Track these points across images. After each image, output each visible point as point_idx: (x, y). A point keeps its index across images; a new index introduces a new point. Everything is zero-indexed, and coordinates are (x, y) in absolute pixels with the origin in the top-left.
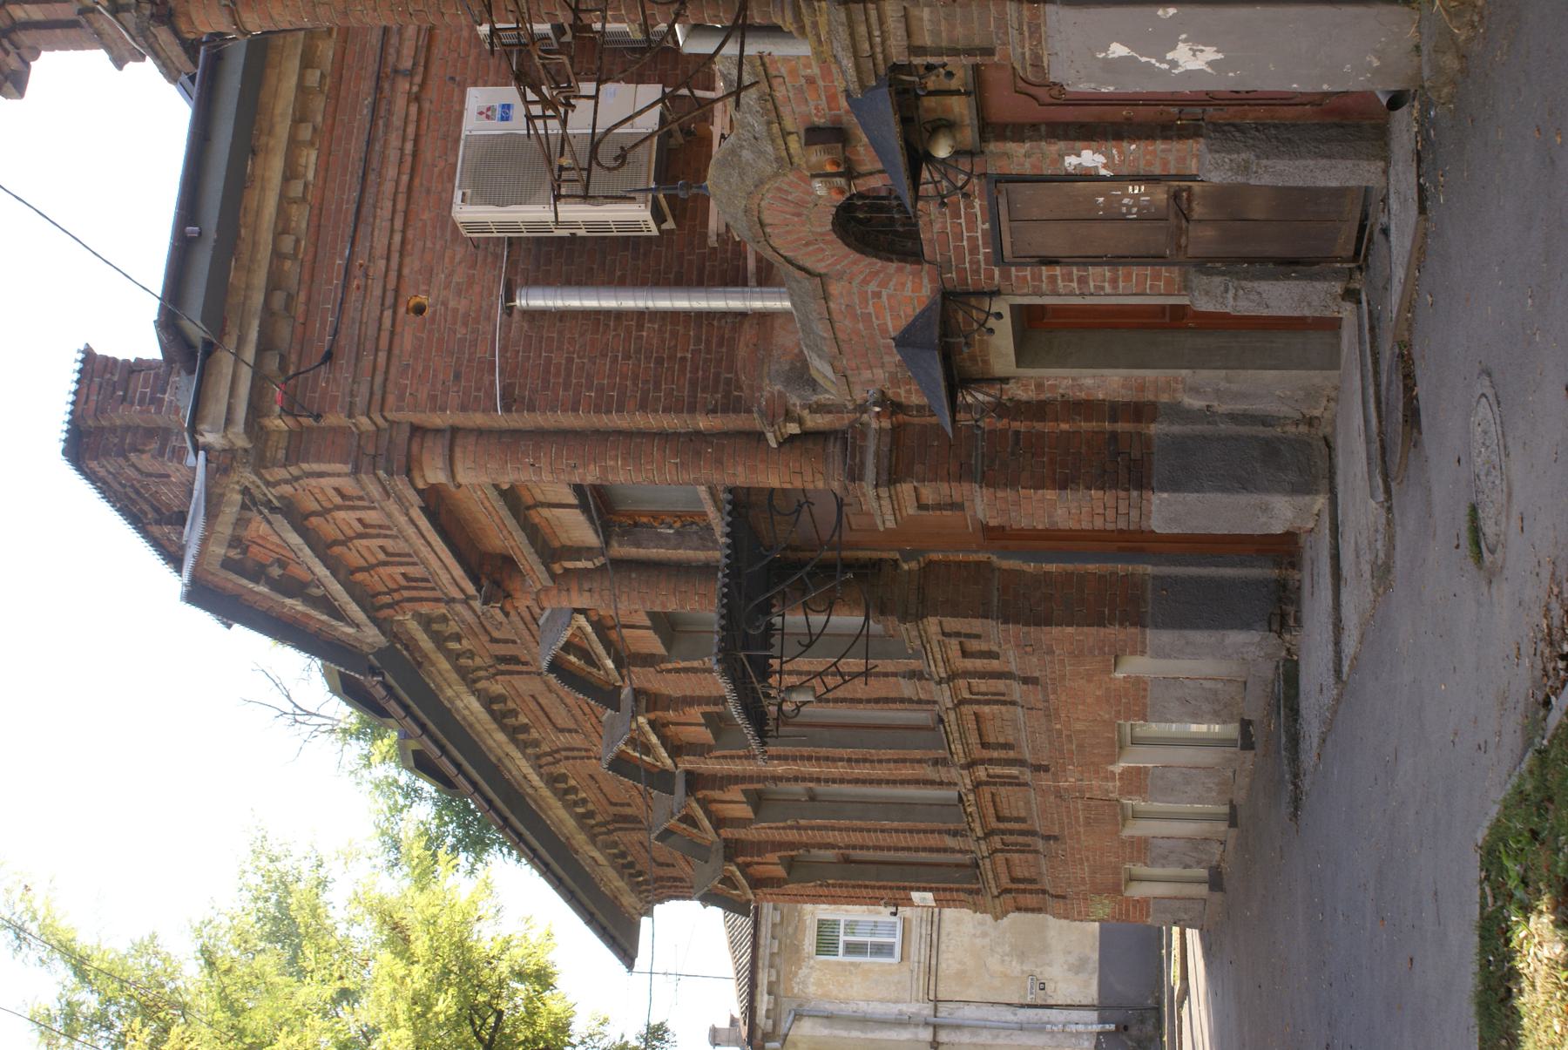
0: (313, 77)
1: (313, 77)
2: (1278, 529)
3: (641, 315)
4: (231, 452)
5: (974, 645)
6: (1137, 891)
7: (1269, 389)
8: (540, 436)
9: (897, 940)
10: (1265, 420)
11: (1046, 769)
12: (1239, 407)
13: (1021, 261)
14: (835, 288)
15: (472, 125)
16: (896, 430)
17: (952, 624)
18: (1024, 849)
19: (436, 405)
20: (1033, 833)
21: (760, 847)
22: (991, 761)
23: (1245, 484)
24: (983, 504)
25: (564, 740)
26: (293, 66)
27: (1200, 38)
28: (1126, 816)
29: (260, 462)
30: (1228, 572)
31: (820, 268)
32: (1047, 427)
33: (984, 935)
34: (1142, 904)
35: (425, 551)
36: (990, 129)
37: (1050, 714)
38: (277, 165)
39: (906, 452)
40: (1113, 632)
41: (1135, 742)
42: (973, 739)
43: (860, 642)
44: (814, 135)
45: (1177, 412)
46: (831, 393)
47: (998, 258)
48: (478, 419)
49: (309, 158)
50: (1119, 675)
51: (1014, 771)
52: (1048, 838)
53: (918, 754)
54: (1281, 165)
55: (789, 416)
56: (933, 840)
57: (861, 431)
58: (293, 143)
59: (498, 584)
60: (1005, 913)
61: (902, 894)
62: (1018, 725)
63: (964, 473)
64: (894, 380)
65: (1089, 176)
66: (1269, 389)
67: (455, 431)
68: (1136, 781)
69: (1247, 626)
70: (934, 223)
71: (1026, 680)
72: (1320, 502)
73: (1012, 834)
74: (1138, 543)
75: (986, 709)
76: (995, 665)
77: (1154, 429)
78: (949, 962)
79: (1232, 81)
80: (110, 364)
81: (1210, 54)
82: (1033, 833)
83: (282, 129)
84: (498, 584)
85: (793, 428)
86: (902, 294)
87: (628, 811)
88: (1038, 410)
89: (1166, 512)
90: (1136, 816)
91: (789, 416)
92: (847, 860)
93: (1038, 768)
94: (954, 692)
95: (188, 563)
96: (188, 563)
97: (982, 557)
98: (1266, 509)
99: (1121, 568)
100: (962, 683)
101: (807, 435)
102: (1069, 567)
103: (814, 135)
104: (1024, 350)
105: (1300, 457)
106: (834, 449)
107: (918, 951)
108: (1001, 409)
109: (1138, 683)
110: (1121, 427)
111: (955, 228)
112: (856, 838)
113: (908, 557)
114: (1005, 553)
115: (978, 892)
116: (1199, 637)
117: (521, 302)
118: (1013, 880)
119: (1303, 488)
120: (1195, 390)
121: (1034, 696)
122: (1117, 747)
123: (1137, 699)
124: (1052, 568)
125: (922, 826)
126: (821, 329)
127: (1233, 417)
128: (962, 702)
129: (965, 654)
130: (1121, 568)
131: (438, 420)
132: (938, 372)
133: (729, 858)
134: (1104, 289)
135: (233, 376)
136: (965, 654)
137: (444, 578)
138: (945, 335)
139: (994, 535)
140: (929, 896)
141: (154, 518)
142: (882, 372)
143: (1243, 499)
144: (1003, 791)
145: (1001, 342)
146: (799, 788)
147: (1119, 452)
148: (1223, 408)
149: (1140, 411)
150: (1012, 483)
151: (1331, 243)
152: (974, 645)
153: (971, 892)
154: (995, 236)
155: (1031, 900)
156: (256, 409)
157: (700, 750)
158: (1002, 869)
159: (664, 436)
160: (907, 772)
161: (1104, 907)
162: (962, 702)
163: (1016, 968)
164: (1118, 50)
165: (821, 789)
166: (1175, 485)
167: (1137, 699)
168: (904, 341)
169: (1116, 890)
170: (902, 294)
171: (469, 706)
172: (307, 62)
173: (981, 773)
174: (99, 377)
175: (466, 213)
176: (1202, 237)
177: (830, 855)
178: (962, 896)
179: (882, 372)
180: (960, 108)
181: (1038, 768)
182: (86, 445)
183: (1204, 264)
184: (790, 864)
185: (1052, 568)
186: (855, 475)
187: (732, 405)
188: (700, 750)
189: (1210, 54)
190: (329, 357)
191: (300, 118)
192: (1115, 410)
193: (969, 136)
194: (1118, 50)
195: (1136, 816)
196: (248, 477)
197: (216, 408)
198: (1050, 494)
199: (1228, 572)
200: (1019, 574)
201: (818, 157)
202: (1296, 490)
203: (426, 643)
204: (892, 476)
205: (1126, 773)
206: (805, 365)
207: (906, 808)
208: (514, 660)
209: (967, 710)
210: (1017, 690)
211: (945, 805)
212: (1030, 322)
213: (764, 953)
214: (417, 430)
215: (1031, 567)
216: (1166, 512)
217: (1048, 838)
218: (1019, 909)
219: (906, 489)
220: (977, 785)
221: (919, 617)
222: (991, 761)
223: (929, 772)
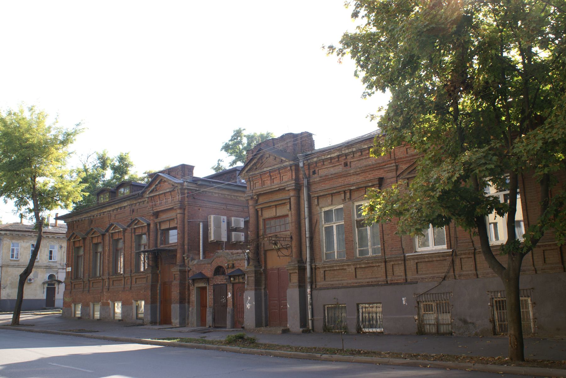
0: (226, 196)
1: (226, 196)
2: (172, 321)
3: (199, 238)
4: (183, 185)
6: (73, 305)
8: (184, 225)
9: (14, 259)
10: (188, 318)
12: (190, 315)
14: (209, 265)
15: (222, 217)
16: (185, 271)
19: (188, 212)
26: (228, 193)
27: (251, 307)
29: (181, 189)
30: (158, 315)
31: (213, 263)
32: (187, 290)
36: (233, 284)
38: (217, 192)
39: (183, 273)
44: (233, 264)
45: (189, 307)
46: (190, 263)
47: (214, 285)
48: (186, 217)
49: (217, 195)
54: (230, 317)
58: (219, 193)
64: (194, 271)
65: (227, 295)
66: (193, 317)
67: (184, 214)
77: (187, 304)
78: (10, 269)
79: (245, 310)
80: (193, 169)
81: (249, 308)
83: (221, 192)
85: (186, 258)
87: (94, 223)
92: (78, 257)
95: (166, 176)
96: (166, 176)
97: (159, 281)
98: (176, 319)
102: (158, 294)
103: (233, 264)
104: (199, 288)
105: (183, 322)
107: (12, 263)
117: (201, 223)
119: (180, 324)
120: (193, 309)
131: (186, 212)
135: (193, 187)
138: (203, 278)
141: (170, 171)
147: (184, 300)
148: (190, 313)
151: (218, 323)
153: (71, 278)
155: (69, 287)
156: (188, 189)
159: (184, 241)
163: (8, 283)
164: (249, 298)
166: (180, 307)
169: (73, 302)
171: (125, 204)
172: (228, 195)
174: (190, 169)
175: (212, 217)
180: (237, 281)
182: (183, 167)
186: (180, 266)
187: (189, 250)
189: (249, 308)
190: (194, 198)
191: (222, 194)
193: (233, 282)
194: (249, 298)
196: (180, 187)
197: (189, 185)
198: (178, 291)
199: (158, 315)
202: (180, 322)
203: (140, 201)
205: (109, 303)
209: (123, 278)
211: (95, 274)
212: (205, 288)
213: (13, 233)
214: (184, 209)
215: (158, 288)
217: (89, 291)
219: (178, 273)
220: (103, 280)
221: (151, 273)
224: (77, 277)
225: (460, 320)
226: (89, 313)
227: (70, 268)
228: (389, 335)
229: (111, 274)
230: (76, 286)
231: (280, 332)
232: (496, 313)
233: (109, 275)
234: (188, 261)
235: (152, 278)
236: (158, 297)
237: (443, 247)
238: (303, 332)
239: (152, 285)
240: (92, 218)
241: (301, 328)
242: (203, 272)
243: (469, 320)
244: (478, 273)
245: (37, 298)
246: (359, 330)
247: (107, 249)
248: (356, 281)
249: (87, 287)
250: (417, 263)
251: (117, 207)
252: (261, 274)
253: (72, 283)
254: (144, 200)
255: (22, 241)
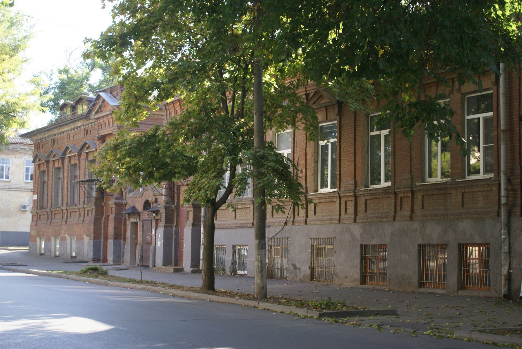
2: (108, 258)
5: (90, 212)
6: (38, 240)
7: (127, 257)
10: (123, 256)
11: (66, 223)
12: (125, 252)
13: (143, 223)
16: (123, 204)
17: (94, 210)
18: (48, 218)
20: (51, 220)
21: (48, 167)
22: (67, 213)
23: (115, 253)
24: (112, 217)
25: (71, 136)
28: (56, 238)
32: (123, 226)
33: (6, 202)
34: (35, 241)
35: (106, 130)
37: (77, 224)
39: (120, 206)
40: (93, 235)
41: (71, 239)
42: (72, 210)
43: (90, 196)
45: (124, 244)
47: (143, 220)
50: (84, 236)
51: (65, 217)
52: (51, 223)
53: (69, 200)
55: (125, 189)
56: (50, 201)
57: (122, 200)
59: (101, 139)
60: (32, 213)
61: (36, 192)
62: (74, 218)
63: (116, 214)
65: (151, 232)
68: (63, 239)
69: (94, 255)
70: (146, 212)
71: (83, 220)
72: (112, 263)
73: (51, 216)
74: (106, 238)
75: (78, 213)
76: (86, 215)
77: (122, 241)
82: (51, 220)
84: (101, 139)
85: (123, 190)
86: (140, 207)
87: (56, 143)
88: (125, 225)
89: (111, 243)
90: (55, 239)
91: (125, 189)
92: (44, 182)
93: (66, 222)
94: (81, 208)
99: (102, 236)
100: (83, 209)
101: (122, 192)
104: (132, 223)
106: (120, 196)
108: (125, 219)
109: (83, 239)
110: (123, 236)
111: (146, 215)
112: (50, 186)
113: (105, 203)
114: (105, 218)
115: (37, 208)
116: (92, 248)
118: (40, 216)
119: (114, 261)
121: (81, 222)
122: (70, 235)
123: (80, 239)
124: (103, 226)
125: (53, 199)
126: (135, 196)
127: (124, 251)
128: (79, 209)
129: (88, 211)
130: (102, 236)
132: (129, 212)
133: (46, 161)
134: (140, 233)
136: (88, 211)
137: (102, 132)
138: (134, 212)
139: (108, 216)
140: (36, 198)
142: (130, 204)
143: (112, 253)
144: (61, 215)
145: (133, 220)
146: (61, 176)
147: (119, 236)
149: (125, 239)
150: (115, 221)
152: (90, 212)
153: (37, 207)
154: (146, 220)
155: (35, 218)
157: (70, 161)
158: (43, 213)
160: (65, 198)
161: (34, 233)
162: (79, 209)
165: (61, 181)
166: (114, 243)
167: (80, 239)
168: (134, 207)
169: (38, 235)
170: (140, 207)
173: (65, 211)
176: (145, 246)
177: (46, 179)
178: (36, 205)
179: (130, 204)
181: (66, 222)
183: (142, 246)
184: (44, 172)
185: (103, 226)
186: (116, 199)
188: (70, 161)
192: (125, 235)
193: (156, 218)
195: (55, 239)
200: (102, 220)
201: (154, 199)
204: (116, 204)
206: (132, 192)
207: (57, 196)
208: (87, 133)
209: (78, 210)
210: (82, 219)
211: (57, 204)
212: (136, 223)
215: (103, 222)
216: (111, 243)
217: (51, 223)
218: (33, 216)
219: (114, 206)
220: (62, 210)
222: (67, 213)
223: (65, 202)
224: (42, 208)
225: (292, 265)
226: (51, 249)
227: (36, 196)
228: (249, 277)
229: (69, 204)
230: (42, 217)
231: (172, 271)
232: (315, 259)
233: (67, 205)
234: (126, 194)
235: (96, 210)
236: (103, 232)
237: (389, 184)
238: (193, 272)
239: (95, 219)
240: (54, 137)
241: (191, 267)
242: (136, 206)
243: (298, 266)
244: (308, 220)
245: (20, 230)
246: (234, 272)
247: (66, 175)
248: (235, 222)
249: (50, 219)
250: (463, 193)
251: (73, 127)
252: (173, 210)
253: (37, 214)
254: (91, 121)
255: (13, 156)
